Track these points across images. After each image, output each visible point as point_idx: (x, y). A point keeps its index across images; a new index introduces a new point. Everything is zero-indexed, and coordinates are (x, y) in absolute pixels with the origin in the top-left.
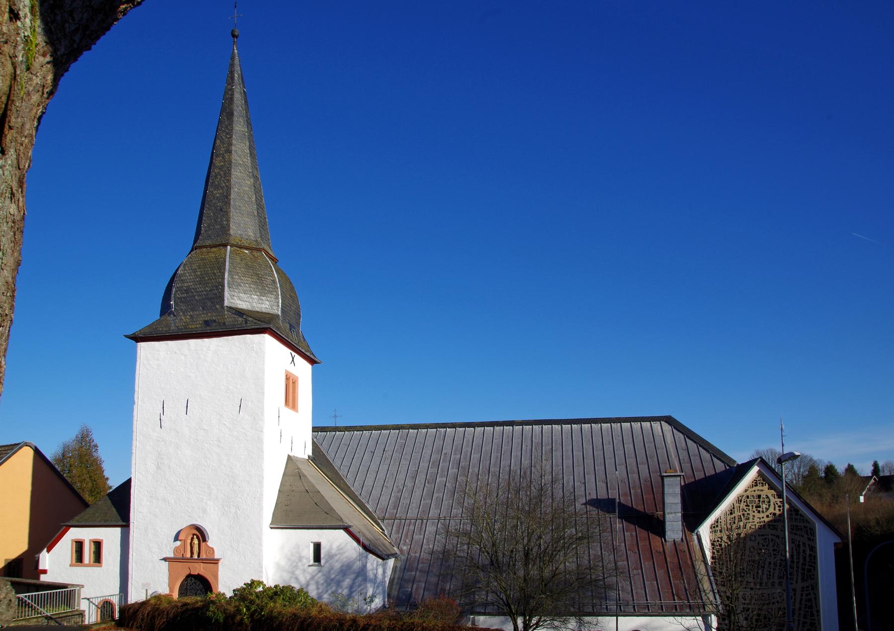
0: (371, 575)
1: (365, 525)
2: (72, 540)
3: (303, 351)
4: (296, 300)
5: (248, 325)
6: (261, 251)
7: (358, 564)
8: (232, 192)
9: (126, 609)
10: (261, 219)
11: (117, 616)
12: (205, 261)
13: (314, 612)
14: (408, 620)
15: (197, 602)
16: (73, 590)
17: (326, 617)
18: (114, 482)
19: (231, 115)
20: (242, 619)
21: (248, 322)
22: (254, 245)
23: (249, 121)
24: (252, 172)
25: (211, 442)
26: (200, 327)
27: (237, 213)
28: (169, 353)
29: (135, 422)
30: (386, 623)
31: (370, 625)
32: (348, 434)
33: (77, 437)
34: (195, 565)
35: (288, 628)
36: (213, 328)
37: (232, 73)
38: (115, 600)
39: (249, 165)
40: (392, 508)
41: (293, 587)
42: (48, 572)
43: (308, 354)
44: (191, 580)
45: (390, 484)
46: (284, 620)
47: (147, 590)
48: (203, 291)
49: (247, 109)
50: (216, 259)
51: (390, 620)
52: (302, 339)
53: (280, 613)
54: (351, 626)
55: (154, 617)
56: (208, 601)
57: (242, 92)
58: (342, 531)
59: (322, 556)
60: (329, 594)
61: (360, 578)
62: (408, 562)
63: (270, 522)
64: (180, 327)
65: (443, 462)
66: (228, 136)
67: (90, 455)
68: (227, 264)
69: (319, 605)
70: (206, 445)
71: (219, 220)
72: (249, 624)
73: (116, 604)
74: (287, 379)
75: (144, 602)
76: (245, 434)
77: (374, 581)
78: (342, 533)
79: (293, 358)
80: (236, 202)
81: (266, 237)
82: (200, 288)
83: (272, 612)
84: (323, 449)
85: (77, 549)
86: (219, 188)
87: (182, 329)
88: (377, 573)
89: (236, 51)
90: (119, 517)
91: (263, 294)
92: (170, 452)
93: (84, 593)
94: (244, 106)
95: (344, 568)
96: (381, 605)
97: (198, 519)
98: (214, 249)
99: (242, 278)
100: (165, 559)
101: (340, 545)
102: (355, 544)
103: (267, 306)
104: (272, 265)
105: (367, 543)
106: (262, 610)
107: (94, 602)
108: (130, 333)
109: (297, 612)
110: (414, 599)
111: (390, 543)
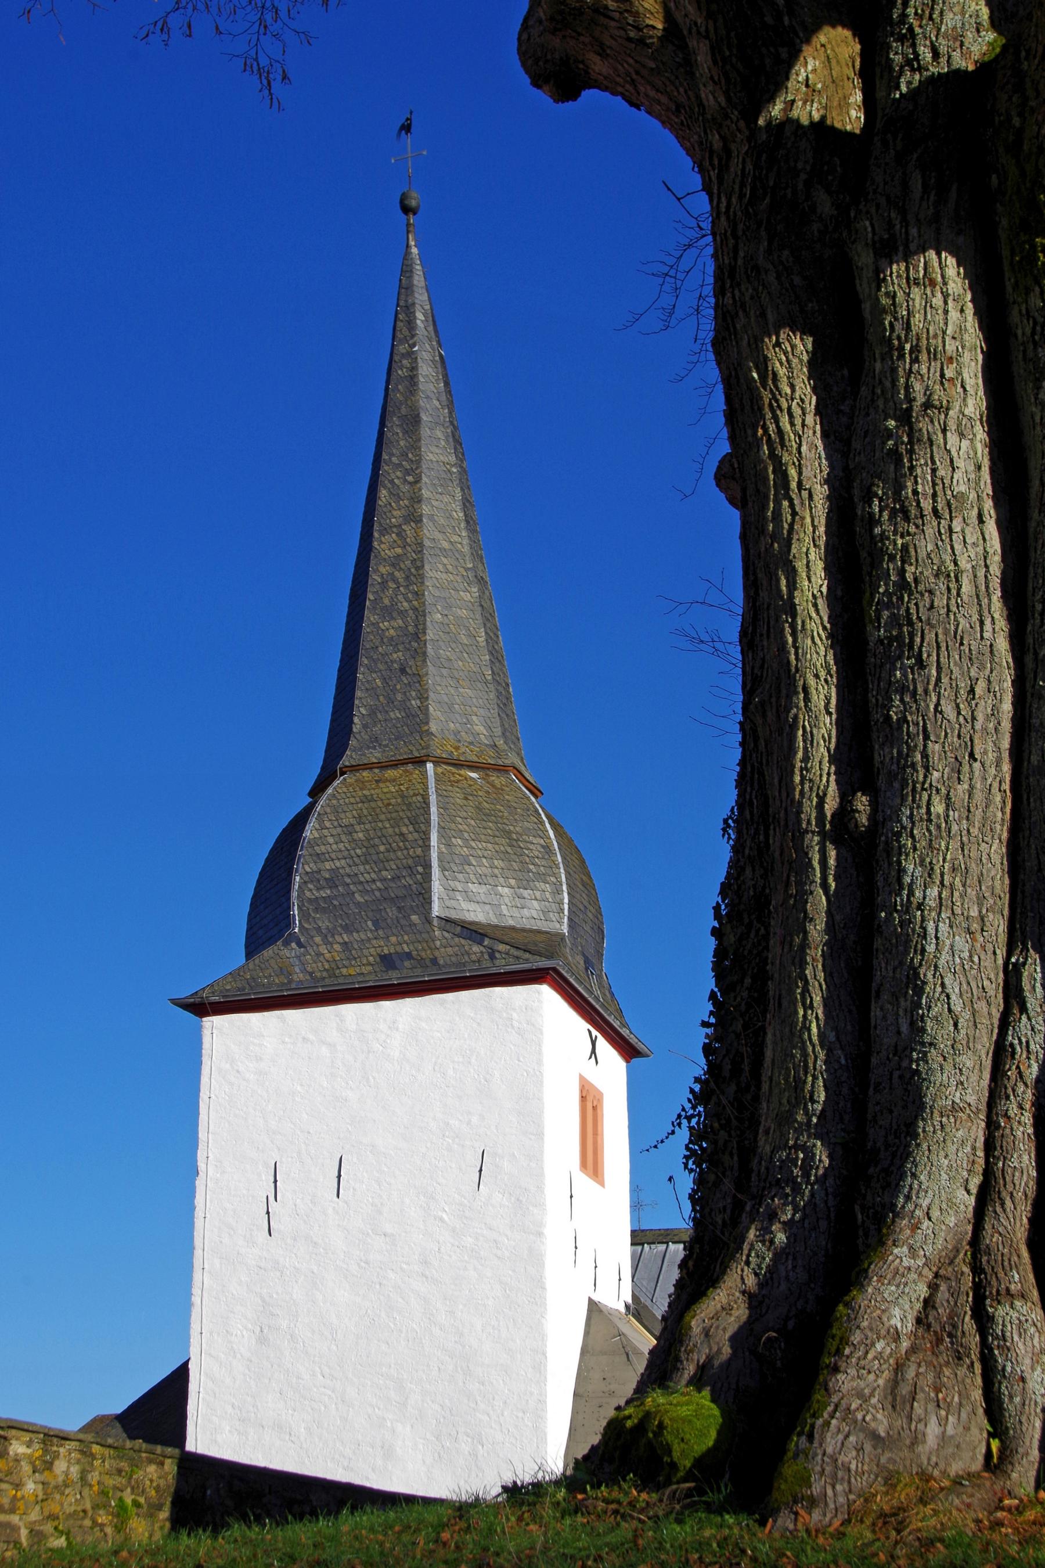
5: (497, 962)
8: (428, 624)
12: (373, 804)
19: (413, 421)
21: (497, 955)
23: (457, 434)
25: (404, 1266)
26: (370, 973)
29: (199, 1223)
36: (405, 973)
39: (466, 549)
48: (374, 881)
49: (451, 406)
50: (403, 797)
57: (437, 358)
64: (319, 974)
66: (410, 479)
68: (434, 809)
70: (391, 1275)
71: (399, 697)
76: (495, 1241)
86: (395, 614)
87: (324, 978)
89: (415, 251)
91: (525, 883)
92: (295, 1296)
94: (444, 398)
98: (390, 773)
103: (535, 914)
108: (184, 992)
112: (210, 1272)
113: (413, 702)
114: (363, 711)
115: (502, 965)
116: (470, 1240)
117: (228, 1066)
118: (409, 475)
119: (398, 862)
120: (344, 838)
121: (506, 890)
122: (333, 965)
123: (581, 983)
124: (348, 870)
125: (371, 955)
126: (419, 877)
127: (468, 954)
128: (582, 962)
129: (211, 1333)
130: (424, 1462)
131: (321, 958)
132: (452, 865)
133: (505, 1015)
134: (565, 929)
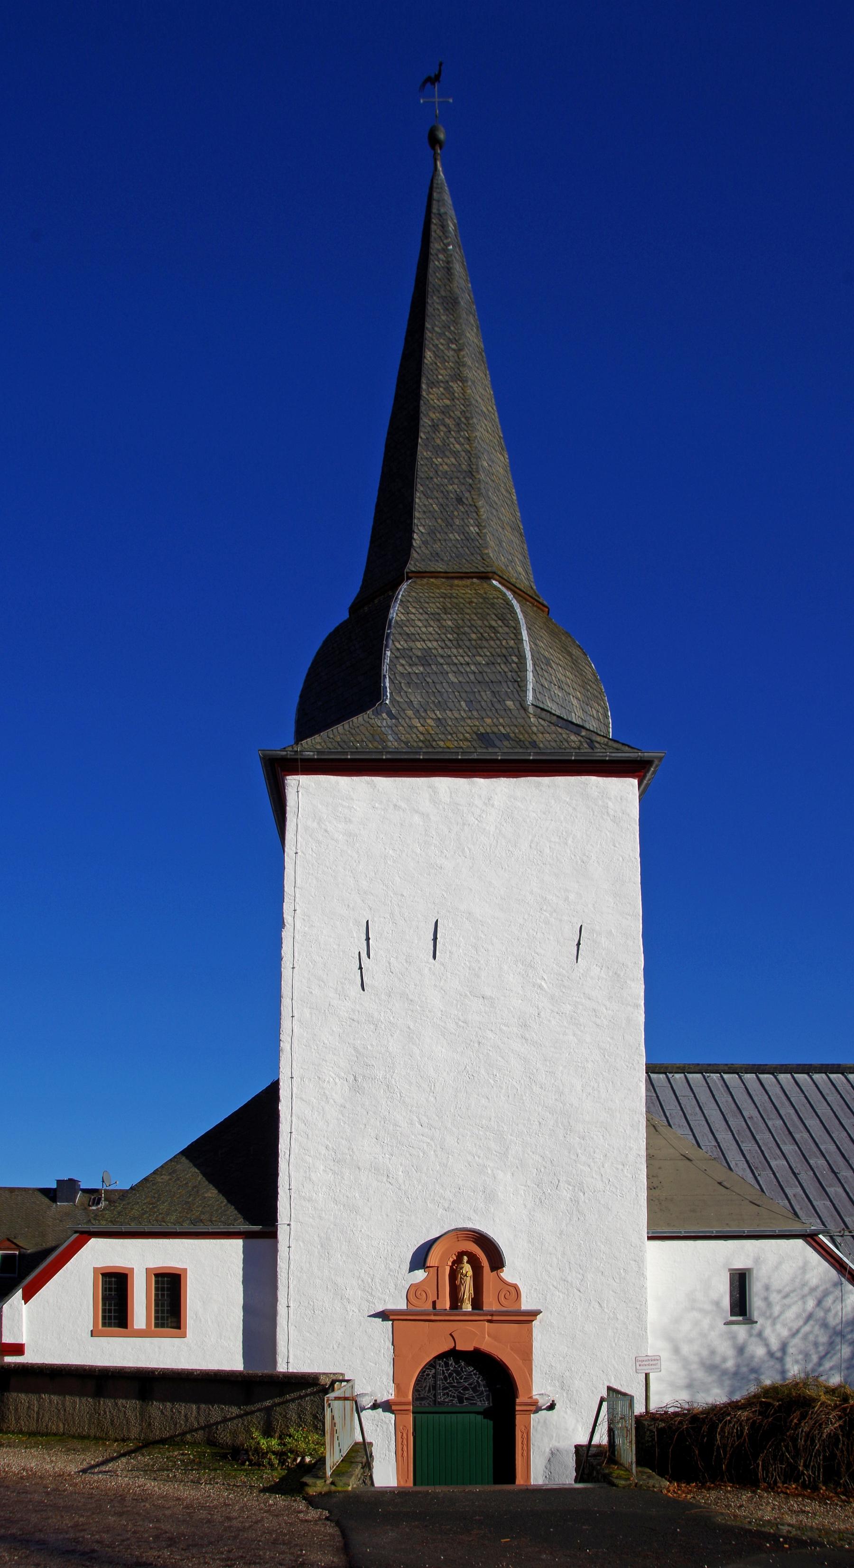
2: (95, 1269)
19: (451, 303)
25: (504, 1028)
34: (469, 1326)
42: (27, 1350)
44: (447, 1365)
48: (468, 664)
58: (800, 1242)
70: (490, 1035)
71: (457, 522)
76: (594, 1010)
92: (391, 1049)
100: (384, 1315)
112: (300, 1021)
113: (471, 528)
117: (315, 825)
118: (452, 343)
122: (428, 737)
126: (514, 666)
129: (302, 1078)
130: (525, 1206)
133: (600, 802)
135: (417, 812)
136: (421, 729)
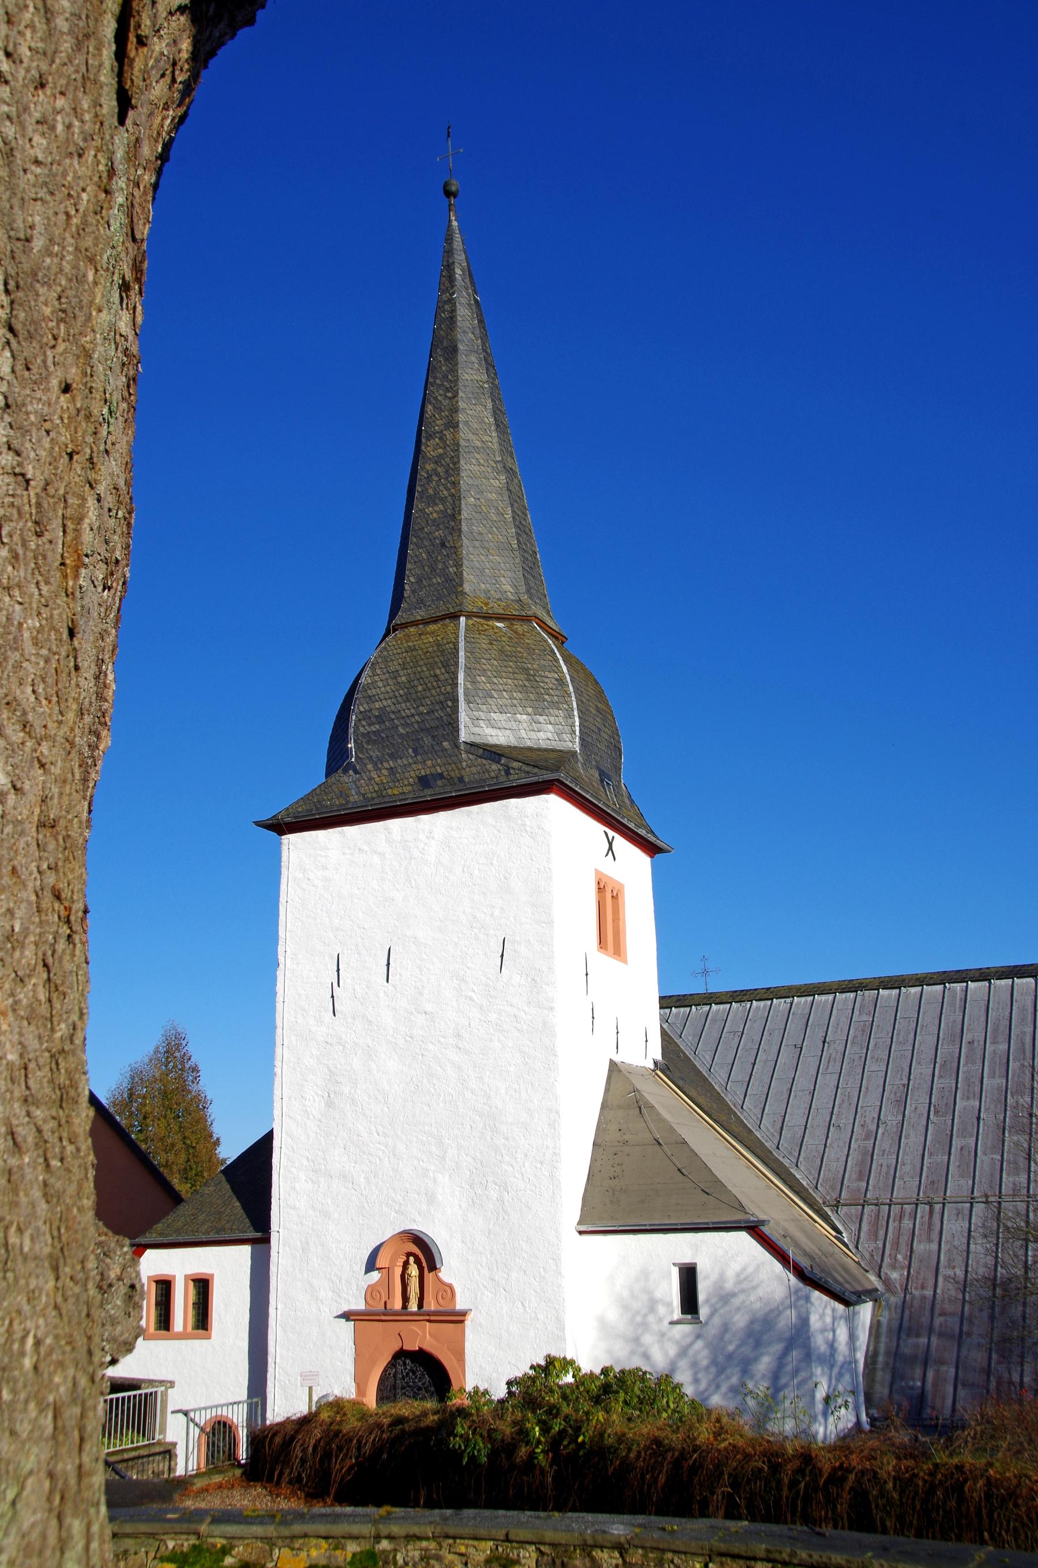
0: (820, 1343)
1: (795, 1220)
3: (632, 826)
4: (610, 717)
5: (511, 777)
6: (530, 621)
7: (789, 1318)
8: (463, 506)
9: (267, 1436)
10: (526, 555)
11: (242, 1453)
12: (414, 653)
13: (704, 1434)
14: (945, 1459)
15: (425, 1414)
16: (151, 1394)
17: (734, 1446)
18: (230, 1151)
19: (452, 351)
20: (532, 1455)
21: (512, 771)
22: (515, 610)
23: (490, 359)
24: (502, 461)
25: (442, 1039)
26: (410, 792)
27: (474, 547)
28: (347, 851)
29: (279, 1006)
30: (888, 1465)
31: (849, 1470)
32: (738, 1008)
33: (156, 1051)
35: (643, 1476)
36: (437, 790)
37: (449, 267)
38: (239, 1417)
39: (496, 446)
40: (854, 1176)
41: (645, 1373)
43: (642, 832)
44: (405, 1364)
45: (844, 1119)
46: (632, 1455)
47: (310, 1388)
48: (413, 715)
49: (484, 338)
50: (438, 645)
51: (898, 1458)
52: (627, 801)
53: (621, 1438)
54: (800, 1471)
55: (327, 1455)
56: (451, 1411)
59: (701, 1297)
60: (726, 1394)
61: (795, 1354)
62: (907, 1313)
63: (577, 1217)
64: (369, 795)
65: (966, 1063)
66: (449, 395)
67: (184, 1090)
68: (462, 653)
69: (713, 1417)
70: (431, 1047)
71: (440, 566)
72: (547, 1468)
73: (240, 1424)
74: (601, 889)
75: (305, 1417)
77: (829, 1359)
78: (743, 1238)
79: (610, 844)
80: (473, 524)
81: (538, 591)
82: (407, 709)
83: (601, 1435)
84: (685, 1044)
85: (159, 1299)
86: (437, 501)
87: (373, 799)
88: (834, 1340)
89: (455, 224)
90: (247, 1220)
91: (540, 710)
93: (176, 1399)
94: (477, 332)
95: (757, 1327)
96: (850, 1425)
97: (419, 1219)
98: (432, 627)
99: (495, 680)
100: (347, 1316)
101: (744, 1269)
102: (778, 1266)
103: (550, 736)
104: (554, 647)
105: (804, 1263)
106: (578, 1430)
107: (197, 1420)
108: (266, 816)
109: (661, 1434)
110: (933, 1408)
111: (858, 1263)
114: (412, 580)
115: (517, 779)
116: (495, 1016)
117: (301, 875)
119: (432, 698)
120: (390, 682)
121: (524, 717)
123: (587, 792)
124: (393, 708)
125: (411, 777)
127: (488, 772)
128: (597, 775)
131: (372, 782)
132: (477, 698)
133: (519, 822)
134: (577, 748)
135: (375, 852)
136: (377, 779)
